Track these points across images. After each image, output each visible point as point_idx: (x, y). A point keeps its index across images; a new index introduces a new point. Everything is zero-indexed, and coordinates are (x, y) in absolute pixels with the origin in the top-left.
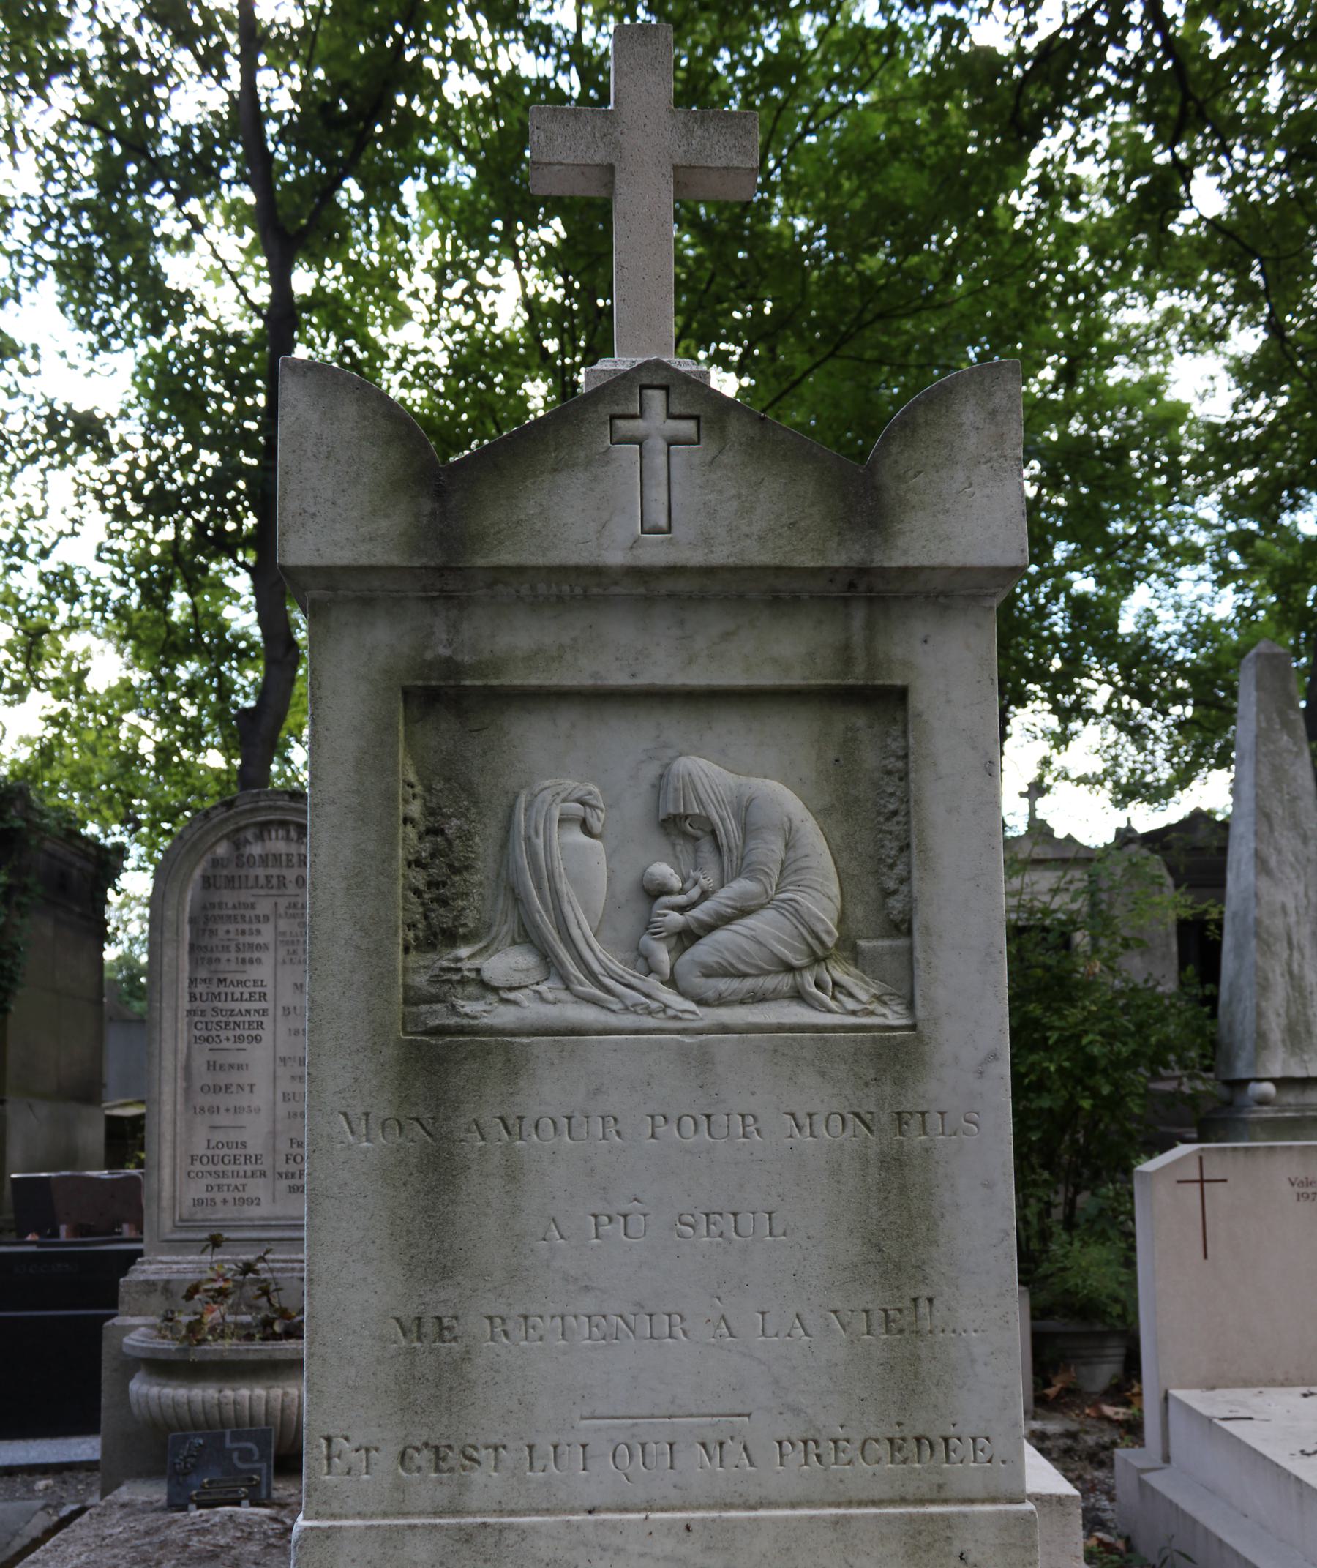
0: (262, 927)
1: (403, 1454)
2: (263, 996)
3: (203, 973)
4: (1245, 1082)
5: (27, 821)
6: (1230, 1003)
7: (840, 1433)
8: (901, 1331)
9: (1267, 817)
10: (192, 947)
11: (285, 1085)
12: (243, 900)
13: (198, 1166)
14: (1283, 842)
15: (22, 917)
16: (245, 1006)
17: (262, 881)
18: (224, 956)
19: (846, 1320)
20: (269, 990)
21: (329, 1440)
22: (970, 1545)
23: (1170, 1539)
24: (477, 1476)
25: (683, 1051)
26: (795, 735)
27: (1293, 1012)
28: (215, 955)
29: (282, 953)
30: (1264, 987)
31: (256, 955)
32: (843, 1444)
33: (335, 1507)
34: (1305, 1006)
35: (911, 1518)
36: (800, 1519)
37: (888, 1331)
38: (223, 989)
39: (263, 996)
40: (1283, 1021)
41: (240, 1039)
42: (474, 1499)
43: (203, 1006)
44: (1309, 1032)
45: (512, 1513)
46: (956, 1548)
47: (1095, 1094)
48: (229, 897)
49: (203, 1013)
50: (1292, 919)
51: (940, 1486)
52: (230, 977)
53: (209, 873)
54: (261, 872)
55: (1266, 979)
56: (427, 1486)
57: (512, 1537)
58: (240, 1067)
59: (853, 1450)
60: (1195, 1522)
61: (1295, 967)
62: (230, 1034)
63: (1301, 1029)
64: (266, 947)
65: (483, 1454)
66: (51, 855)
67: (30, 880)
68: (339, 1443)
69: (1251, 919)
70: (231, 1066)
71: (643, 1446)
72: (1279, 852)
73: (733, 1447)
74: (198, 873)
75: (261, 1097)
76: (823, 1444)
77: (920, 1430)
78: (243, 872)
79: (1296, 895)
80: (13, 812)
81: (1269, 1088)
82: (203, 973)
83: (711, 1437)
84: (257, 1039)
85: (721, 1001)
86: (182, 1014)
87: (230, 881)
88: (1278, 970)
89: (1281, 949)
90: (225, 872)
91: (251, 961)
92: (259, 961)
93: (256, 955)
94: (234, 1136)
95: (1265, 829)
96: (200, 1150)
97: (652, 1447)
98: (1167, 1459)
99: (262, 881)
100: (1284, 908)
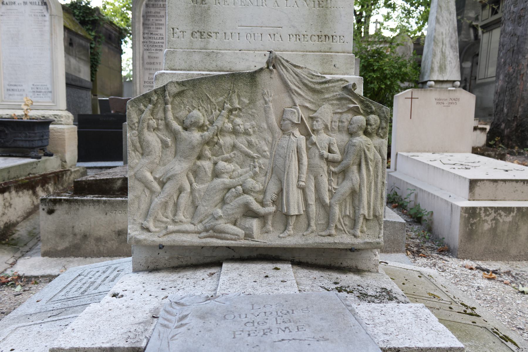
0: (162, 19)
1: (192, 34)
2: (163, 38)
3: (146, 31)
4: (426, 82)
5: (100, 18)
6: (425, 61)
7: (305, 33)
8: (323, 7)
9: (440, 7)
10: (143, 24)
12: (157, 11)
13: (146, 84)
14: (444, 14)
15: (99, 45)
16: (158, 41)
17: (162, 6)
18: (152, 27)
19: (308, 3)
20: (164, 37)
21: (173, 29)
22: (337, 63)
23: (394, 184)
24: (211, 40)
27: (441, 62)
28: (149, 26)
30: (434, 55)
31: (160, 27)
32: (306, 36)
33: (175, 46)
34: (445, 61)
35: (322, 55)
36: (294, 54)
37: (319, 7)
38: (152, 36)
39: (163, 38)
40: (439, 65)
41: (156, 50)
42: (210, 46)
43: (147, 40)
44: (445, 68)
45: (220, 50)
46: (333, 63)
47: (386, 84)
48: (153, 10)
49: (147, 42)
50: (444, 36)
51: (330, 48)
52: (154, 33)
53: (148, 3)
55: (435, 53)
56: (198, 43)
57: (220, 55)
58: (157, 58)
59: (308, 38)
60: (401, 180)
61: (444, 50)
62: (154, 48)
63: (443, 67)
64: (163, 24)
65: (212, 35)
66: (107, 29)
67: (101, 35)
68: (176, 30)
69: (433, 36)
70: (154, 57)
71: (254, 34)
72: (443, 17)
73: (277, 36)
74: (144, 3)
76: (300, 36)
77: (326, 34)
78: (157, 3)
79: (446, 30)
80: (95, 15)
81: (433, 83)
82: (146, 31)
83: (272, 33)
86: (141, 42)
87: (153, 5)
88: (439, 51)
89: (440, 45)
90: (152, 3)
91: (159, 28)
92: (161, 28)
93: (160, 27)
95: (439, 10)
96: (147, 80)
97: (256, 35)
98: (396, 170)
99: (162, 6)
100: (442, 33)
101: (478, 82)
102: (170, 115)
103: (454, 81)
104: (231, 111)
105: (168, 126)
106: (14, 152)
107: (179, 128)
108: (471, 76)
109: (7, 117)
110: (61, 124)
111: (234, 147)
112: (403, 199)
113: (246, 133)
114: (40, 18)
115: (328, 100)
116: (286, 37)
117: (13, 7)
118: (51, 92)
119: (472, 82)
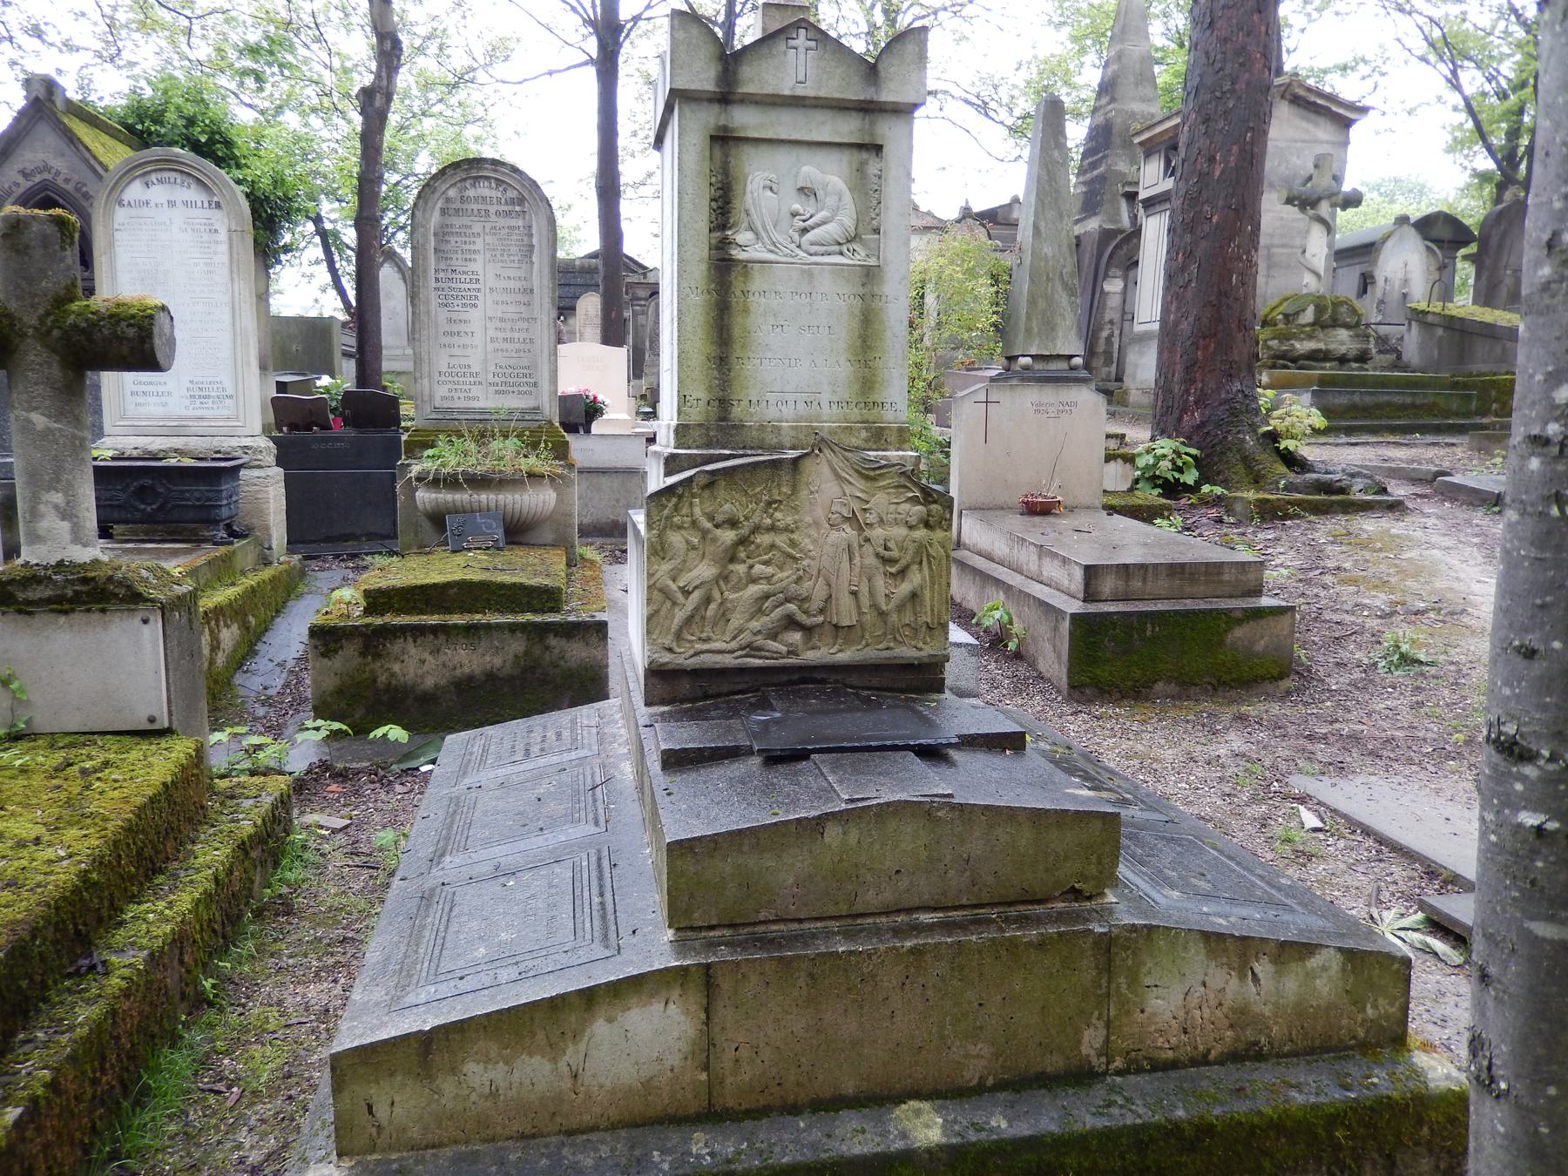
11: (491, 333)
25: (803, 271)
26: (844, 160)
29: (488, 255)
48: (457, 221)
54: (475, 207)
75: (478, 339)
81: (1028, 360)
84: (475, 306)
85: (815, 254)
87: (457, 210)
94: (463, 361)
101: (1138, 328)
102: (697, 511)
103: (1072, 356)
104: (769, 504)
105: (694, 523)
106: (171, 533)
107: (709, 525)
108: (1124, 312)
109: (135, 453)
110: (259, 467)
111: (773, 546)
112: (1414, 1039)
113: (787, 529)
114: (206, 237)
115: (884, 488)
116: (825, 405)
117: (145, 211)
118: (231, 397)
119: (1126, 324)
